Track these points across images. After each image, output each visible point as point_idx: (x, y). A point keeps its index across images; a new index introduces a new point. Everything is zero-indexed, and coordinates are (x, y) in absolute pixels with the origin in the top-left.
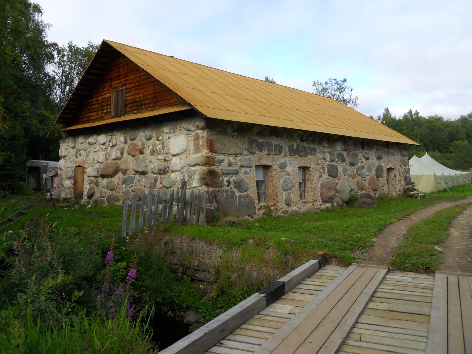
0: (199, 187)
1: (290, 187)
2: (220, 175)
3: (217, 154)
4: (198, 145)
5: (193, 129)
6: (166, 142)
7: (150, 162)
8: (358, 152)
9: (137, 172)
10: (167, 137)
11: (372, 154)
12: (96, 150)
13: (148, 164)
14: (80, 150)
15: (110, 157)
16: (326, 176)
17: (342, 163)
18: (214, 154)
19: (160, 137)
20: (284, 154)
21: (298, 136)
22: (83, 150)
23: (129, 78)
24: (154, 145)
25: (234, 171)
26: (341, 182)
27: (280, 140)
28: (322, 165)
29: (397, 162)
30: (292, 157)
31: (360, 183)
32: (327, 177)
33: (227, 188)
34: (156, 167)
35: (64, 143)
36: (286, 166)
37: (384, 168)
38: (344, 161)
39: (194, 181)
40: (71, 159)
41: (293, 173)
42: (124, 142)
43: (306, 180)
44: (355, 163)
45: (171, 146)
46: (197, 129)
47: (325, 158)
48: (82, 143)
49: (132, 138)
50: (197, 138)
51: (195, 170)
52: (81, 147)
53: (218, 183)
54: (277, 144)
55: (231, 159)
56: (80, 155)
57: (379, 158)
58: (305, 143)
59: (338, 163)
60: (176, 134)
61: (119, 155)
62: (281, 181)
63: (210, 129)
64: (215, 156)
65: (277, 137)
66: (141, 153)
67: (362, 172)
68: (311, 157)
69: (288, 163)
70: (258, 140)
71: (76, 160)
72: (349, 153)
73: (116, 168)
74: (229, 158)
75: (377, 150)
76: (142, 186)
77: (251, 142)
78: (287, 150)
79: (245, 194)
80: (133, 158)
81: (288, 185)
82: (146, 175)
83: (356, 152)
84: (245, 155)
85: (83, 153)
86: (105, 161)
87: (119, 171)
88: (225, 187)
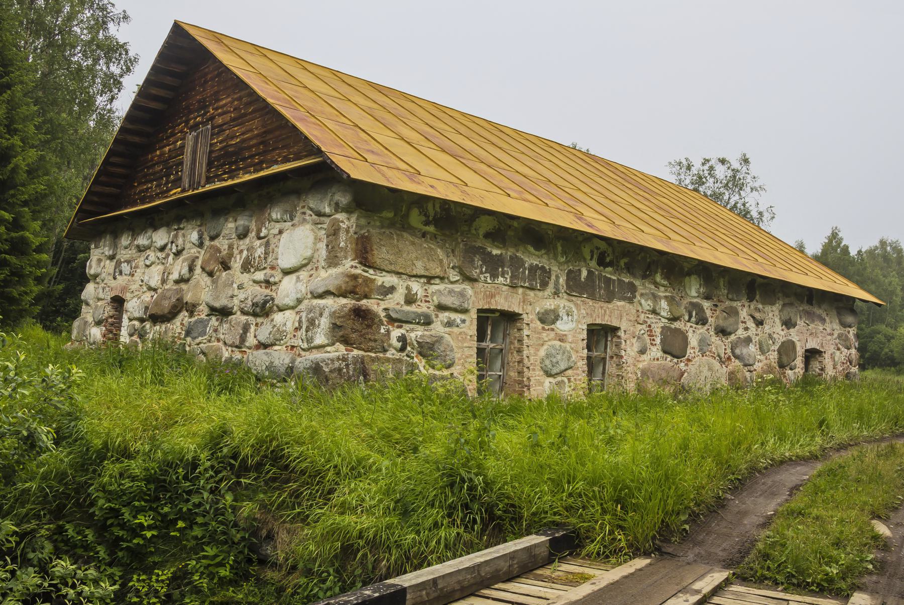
0: (328, 345)
1: (563, 368)
2: (381, 321)
3: (378, 271)
4: (337, 248)
5: (327, 210)
6: (273, 241)
7: (240, 287)
8: (739, 304)
9: (213, 310)
10: (276, 231)
11: (773, 314)
12: (148, 263)
13: (236, 292)
14: (121, 263)
15: (171, 277)
16: (655, 352)
17: (699, 327)
18: (371, 271)
19: (263, 229)
20: (553, 290)
21: (592, 252)
22: (125, 261)
23: (222, 103)
24: (250, 249)
25: (419, 315)
26: (692, 368)
27: (545, 256)
28: (650, 326)
29: (829, 337)
30: (573, 298)
31: (739, 376)
32: (660, 354)
33: (398, 355)
34: (250, 299)
35: (96, 247)
36: (557, 318)
37: (798, 348)
38: (703, 321)
39: (319, 330)
40: (105, 282)
41: (574, 337)
42: (197, 243)
43: (608, 358)
44: (729, 330)
45: (280, 250)
46: (337, 211)
47: (658, 311)
48: (126, 248)
49: (213, 233)
50: (334, 233)
51: (322, 306)
52: (125, 256)
53: (375, 341)
54: (537, 265)
55: (416, 287)
56: (121, 273)
57: (788, 324)
58: (610, 269)
59: (689, 324)
60: (294, 222)
61: (185, 271)
62: (542, 353)
63: (367, 210)
64: (373, 277)
65: (537, 248)
66: (226, 267)
67: (745, 351)
68: (621, 303)
69: (562, 313)
70: (489, 249)
71: (113, 283)
72: (716, 306)
73: (178, 300)
74: (410, 283)
75: (784, 305)
76: (221, 342)
77: (471, 252)
78: (562, 281)
79: (446, 373)
80: (210, 278)
81: (557, 363)
82: (230, 318)
83: (734, 304)
84: (452, 283)
85: (125, 268)
86: (161, 286)
87: (182, 308)
88: (394, 351)
